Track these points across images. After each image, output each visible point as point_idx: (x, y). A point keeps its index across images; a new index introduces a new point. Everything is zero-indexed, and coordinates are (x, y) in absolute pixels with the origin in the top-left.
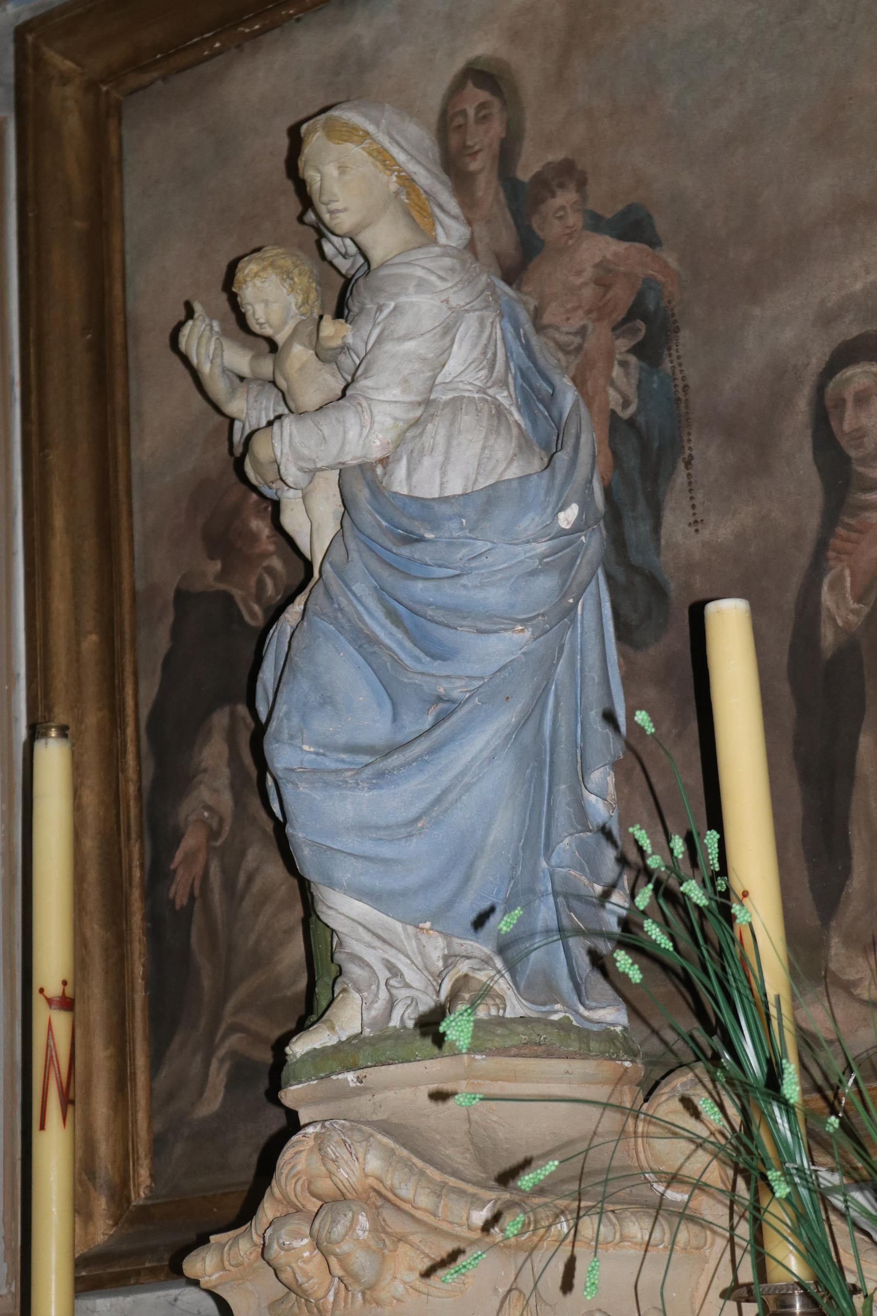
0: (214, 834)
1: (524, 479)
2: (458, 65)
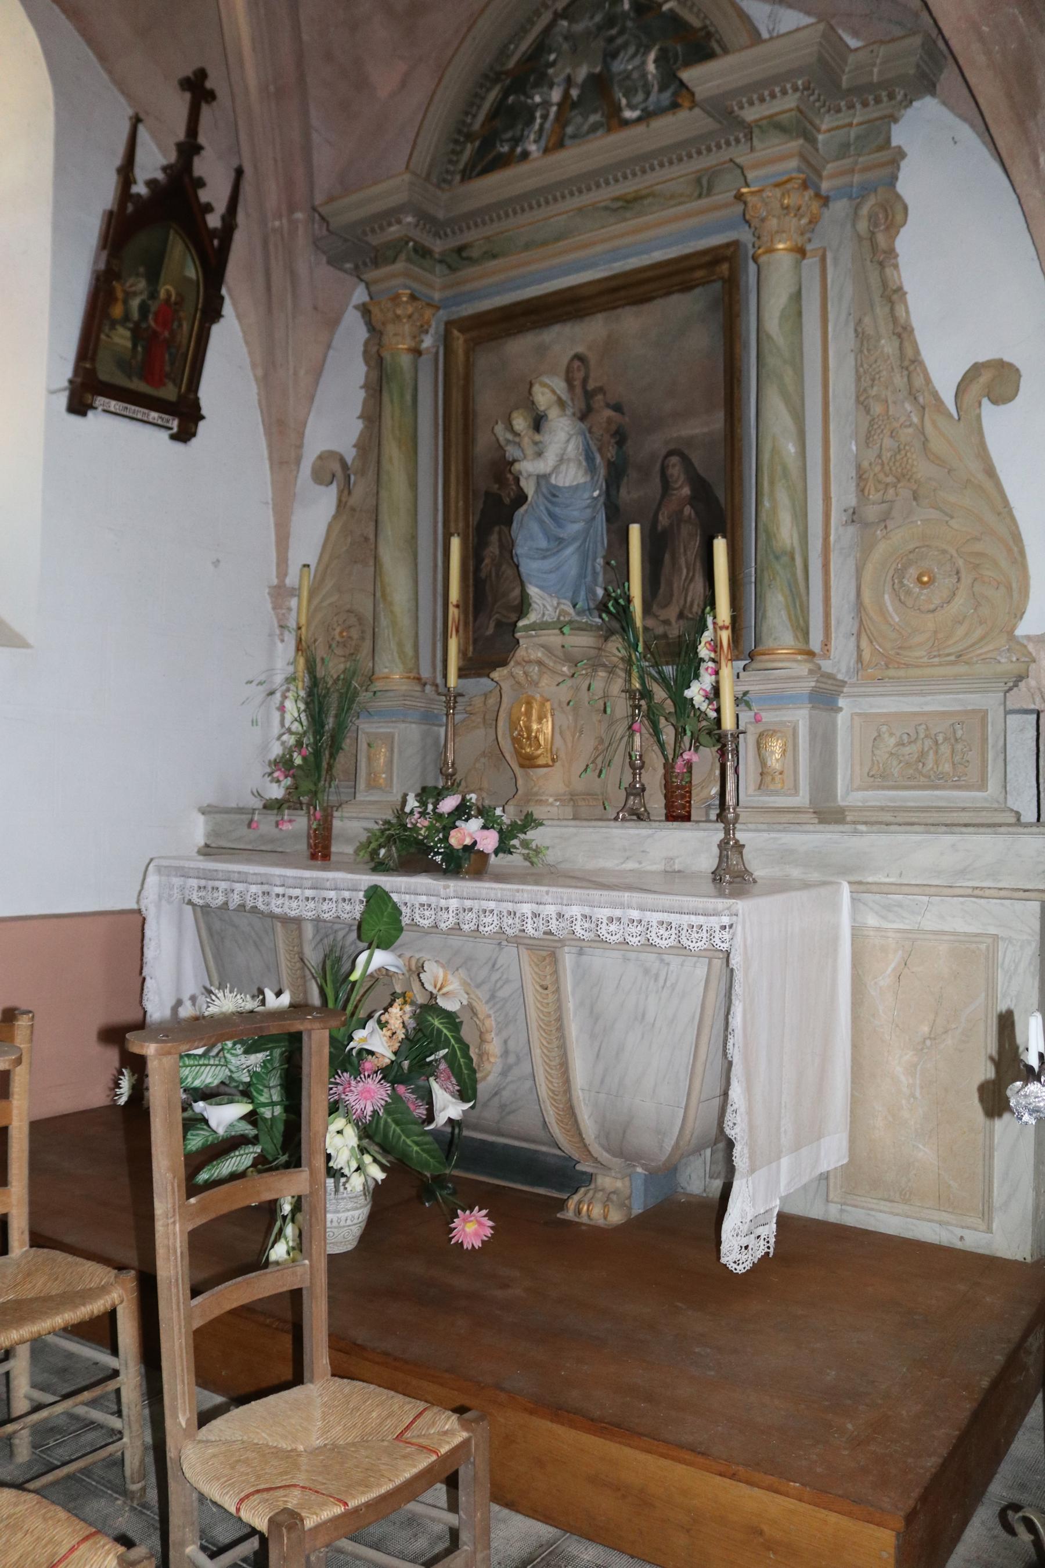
1: (585, 483)
2: (572, 353)
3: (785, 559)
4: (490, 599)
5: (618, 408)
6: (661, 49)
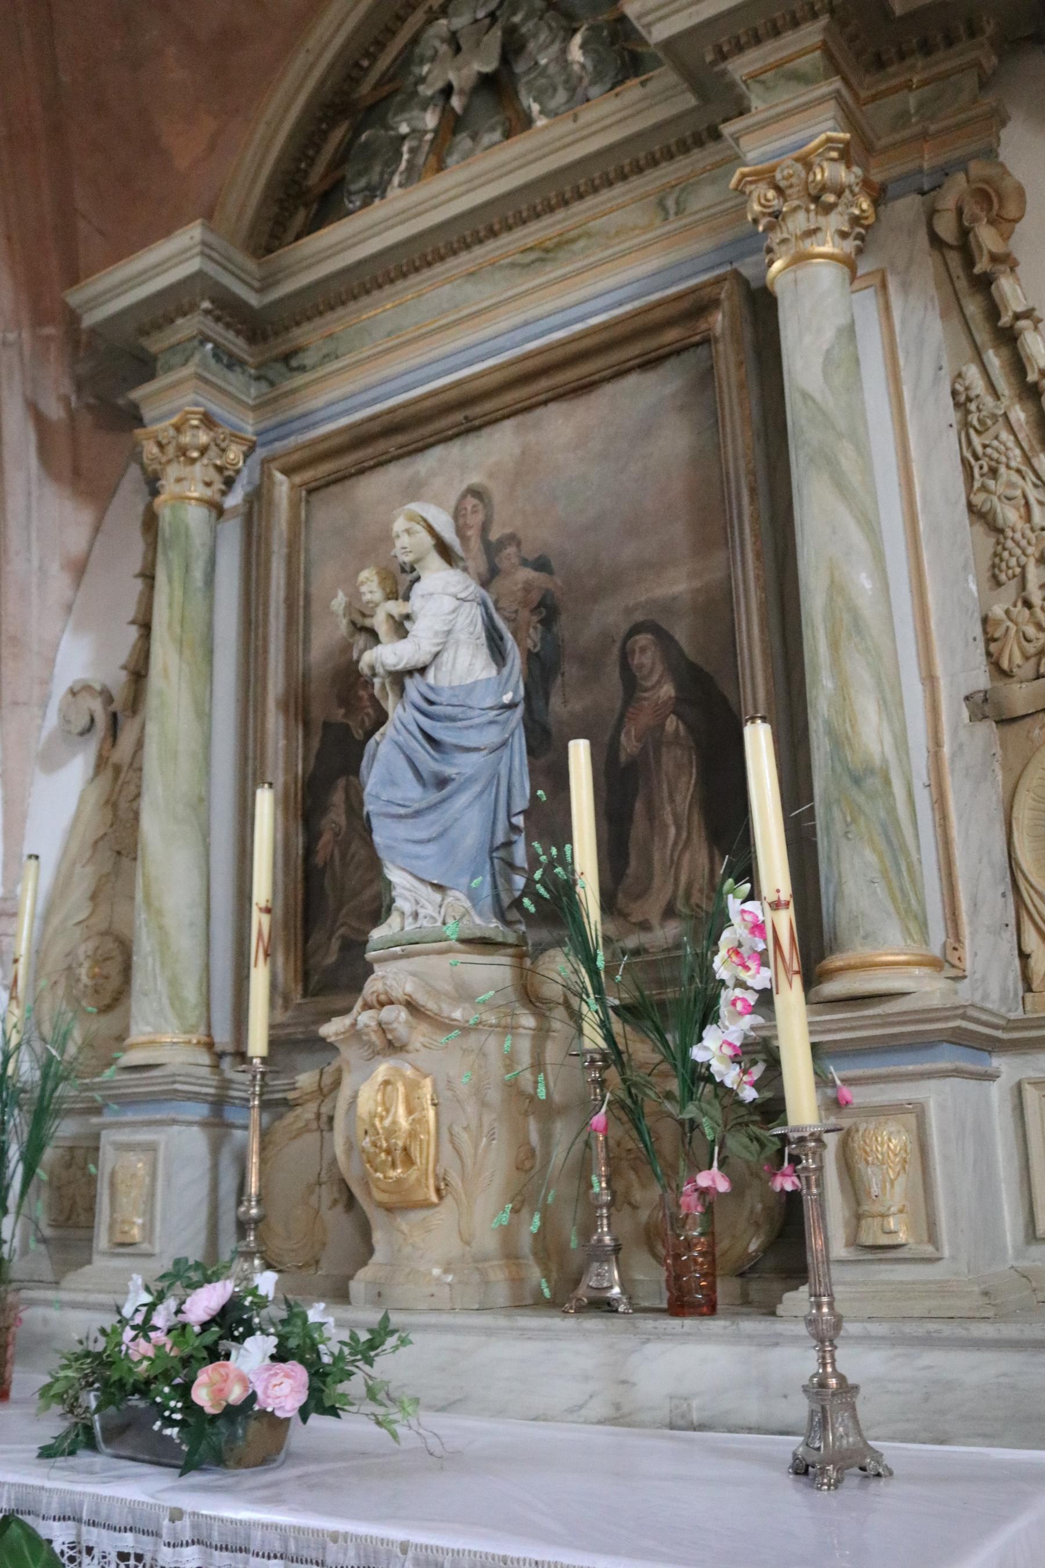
0: (337, 835)
2: (464, 486)
3: (873, 783)
4: (331, 902)
5: (542, 565)
6: (590, 29)
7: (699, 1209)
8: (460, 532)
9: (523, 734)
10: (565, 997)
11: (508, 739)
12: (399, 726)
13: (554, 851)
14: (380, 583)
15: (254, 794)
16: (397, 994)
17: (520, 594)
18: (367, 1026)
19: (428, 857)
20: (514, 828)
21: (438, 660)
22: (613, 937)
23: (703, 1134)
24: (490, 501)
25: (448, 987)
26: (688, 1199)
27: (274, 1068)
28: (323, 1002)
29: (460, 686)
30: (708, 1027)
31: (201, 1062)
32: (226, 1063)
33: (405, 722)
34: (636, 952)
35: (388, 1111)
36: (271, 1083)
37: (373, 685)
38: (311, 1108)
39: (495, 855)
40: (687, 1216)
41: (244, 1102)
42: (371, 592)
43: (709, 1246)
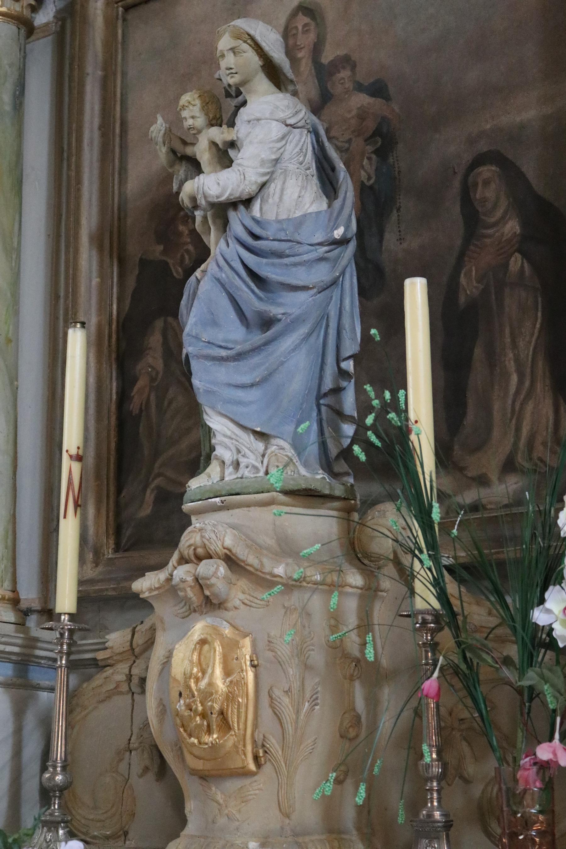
0: (153, 380)
7: (538, 784)
8: (289, 52)
9: (355, 273)
10: (395, 553)
11: (339, 277)
12: (222, 262)
13: (387, 395)
14: (203, 108)
15: (66, 335)
16: (216, 547)
17: (353, 122)
18: (183, 581)
19: (251, 403)
20: (343, 374)
21: (265, 191)
22: (449, 492)
23: (544, 704)
24: (323, 19)
25: (270, 542)
26: (526, 773)
27: (83, 626)
28: (137, 557)
29: (288, 220)
30: (551, 588)
31: (5, 619)
32: (32, 621)
33: (228, 257)
34: (475, 508)
35: (204, 672)
36: (79, 642)
37: (194, 218)
38: (123, 668)
39: (322, 402)
40: (525, 791)
41: (50, 663)
42: (193, 117)
43: (549, 825)
